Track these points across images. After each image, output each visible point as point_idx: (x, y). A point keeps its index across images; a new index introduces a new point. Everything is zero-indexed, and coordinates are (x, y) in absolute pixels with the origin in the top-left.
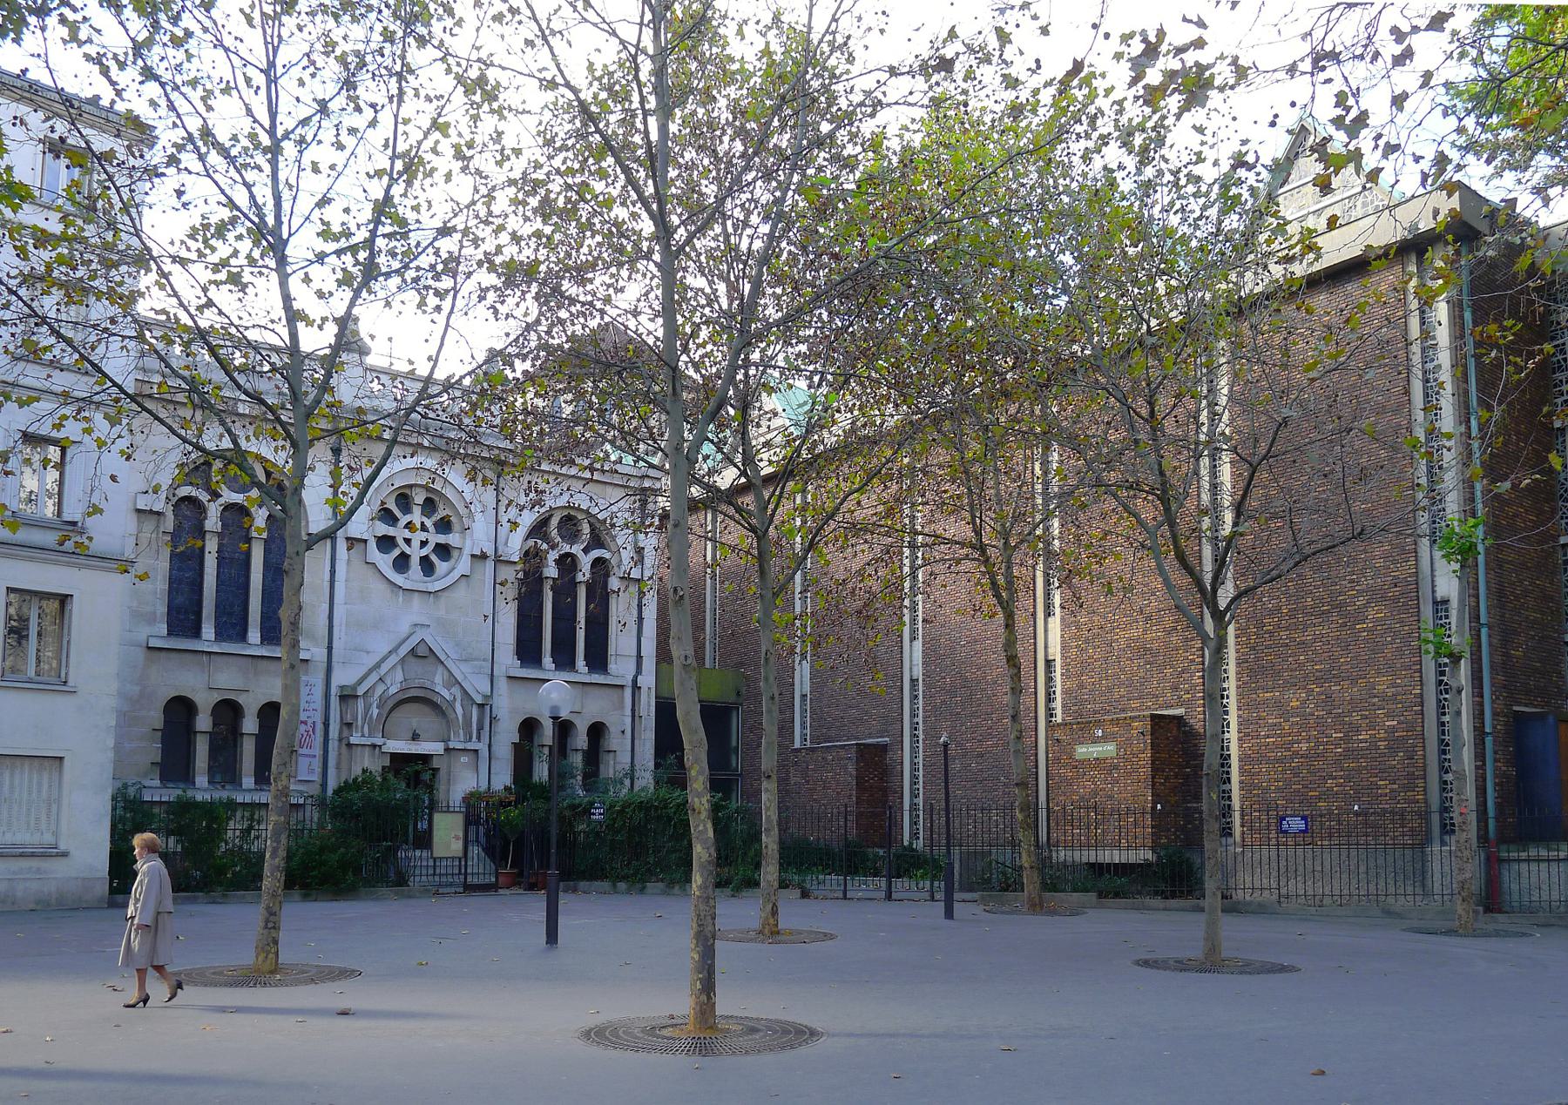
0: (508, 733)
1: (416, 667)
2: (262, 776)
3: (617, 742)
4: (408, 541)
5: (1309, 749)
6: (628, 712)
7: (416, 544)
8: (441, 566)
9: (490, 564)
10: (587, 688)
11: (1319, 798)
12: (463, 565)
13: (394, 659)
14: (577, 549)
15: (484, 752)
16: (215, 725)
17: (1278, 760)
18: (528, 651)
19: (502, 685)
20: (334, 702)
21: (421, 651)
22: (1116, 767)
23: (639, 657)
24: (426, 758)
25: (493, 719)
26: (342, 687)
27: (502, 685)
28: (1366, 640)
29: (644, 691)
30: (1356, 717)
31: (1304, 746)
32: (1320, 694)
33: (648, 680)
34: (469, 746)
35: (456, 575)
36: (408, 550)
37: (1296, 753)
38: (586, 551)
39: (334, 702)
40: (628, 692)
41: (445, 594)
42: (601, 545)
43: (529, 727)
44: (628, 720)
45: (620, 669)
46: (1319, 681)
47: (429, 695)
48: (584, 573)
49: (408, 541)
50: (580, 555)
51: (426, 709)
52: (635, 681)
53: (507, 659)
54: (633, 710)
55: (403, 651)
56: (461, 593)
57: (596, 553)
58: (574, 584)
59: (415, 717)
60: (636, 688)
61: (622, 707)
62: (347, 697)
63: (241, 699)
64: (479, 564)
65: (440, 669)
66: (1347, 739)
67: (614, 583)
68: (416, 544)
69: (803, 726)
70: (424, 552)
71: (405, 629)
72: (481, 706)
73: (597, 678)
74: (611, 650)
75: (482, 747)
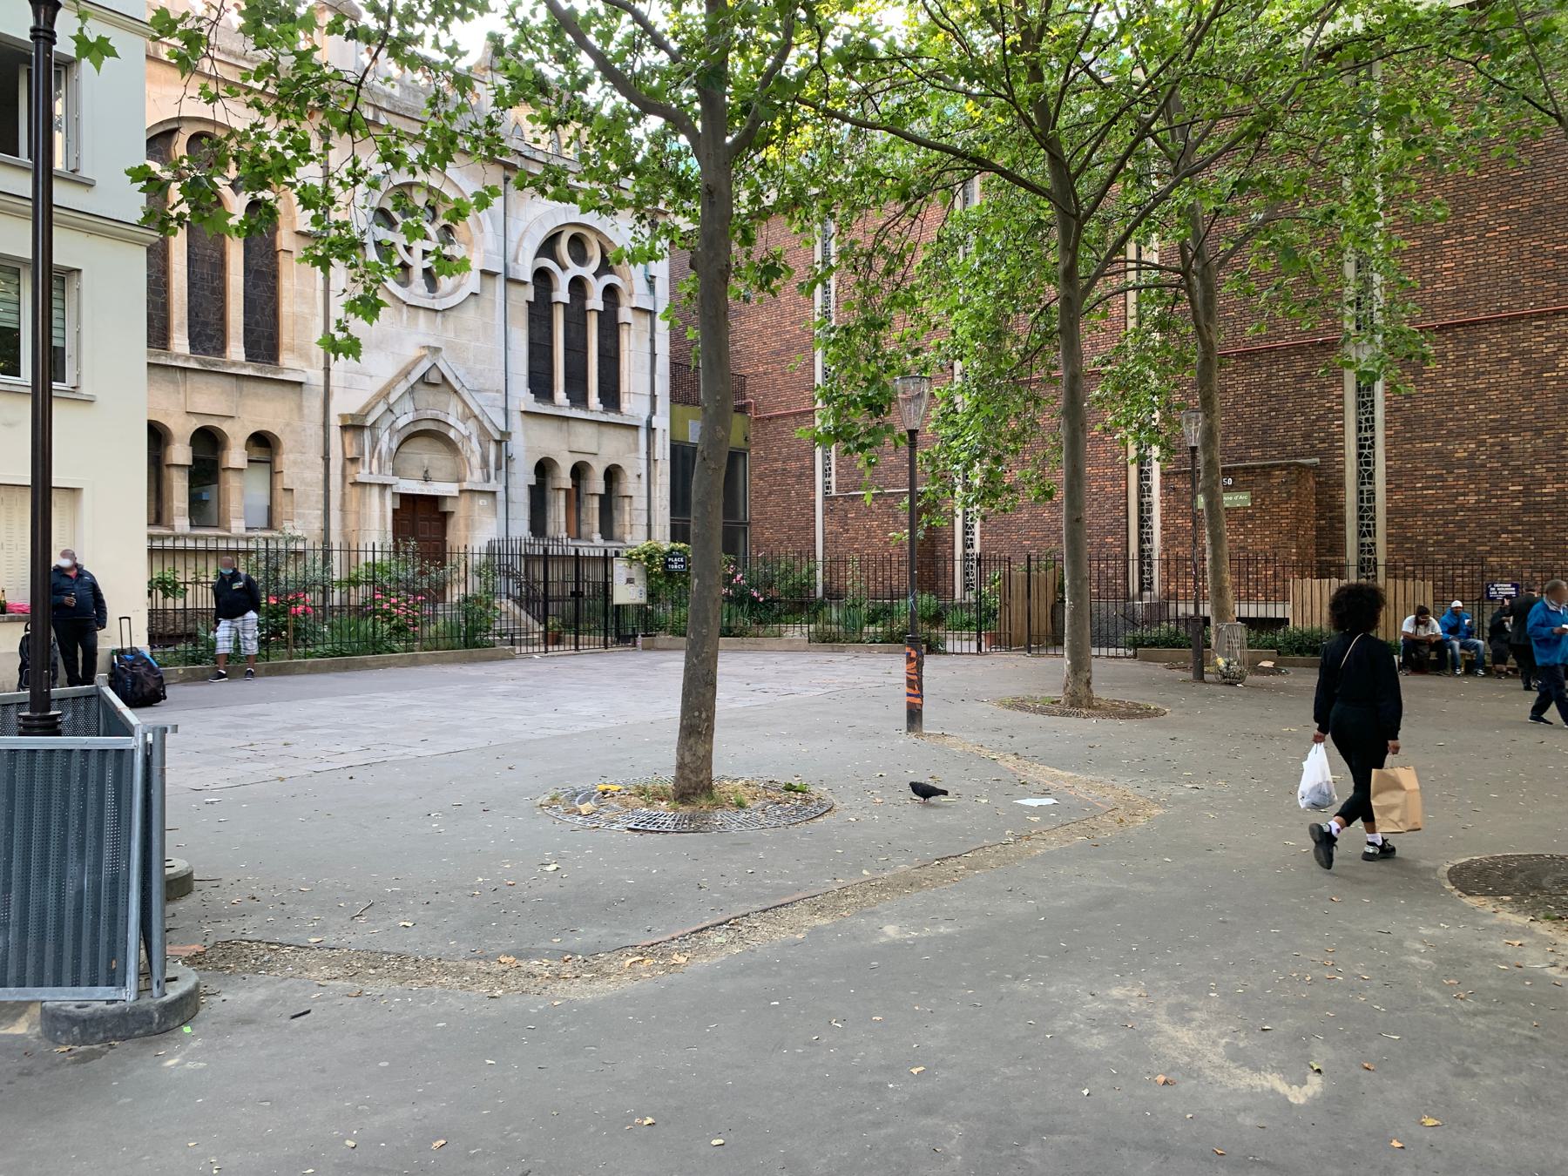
0: (523, 476)
1: (425, 394)
2: (607, 531)
3: (632, 485)
4: (408, 249)
5: (1478, 502)
6: (643, 455)
7: (417, 252)
8: (445, 283)
9: (500, 282)
10: (604, 429)
11: (1490, 553)
12: (472, 281)
13: (403, 387)
14: (587, 272)
15: (501, 496)
16: (195, 459)
17: (1436, 513)
18: (540, 384)
19: (517, 421)
20: (335, 432)
21: (434, 377)
22: (1251, 518)
23: (653, 397)
24: (435, 501)
25: (509, 458)
26: (343, 416)
27: (517, 421)
28: (1554, 390)
29: (659, 434)
30: (1540, 470)
31: (1472, 499)
32: (1493, 445)
33: (662, 422)
34: (487, 487)
35: (463, 293)
36: (409, 260)
37: (1462, 507)
38: (597, 275)
39: (335, 432)
40: (643, 434)
41: (454, 313)
42: (611, 271)
43: (544, 468)
44: (644, 464)
45: (633, 405)
46: (1492, 431)
47: (443, 429)
48: (595, 302)
49: (408, 249)
50: (591, 278)
51: (439, 445)
52: (649, 422)
53: (523, 398)
54: (648, 453)
55: (415, 375)
56: (470, 315)
57: (607, 279)
58: (584, 313)
59: (425, 454)
60: (651, 430)
61: (637, 450)
62: (353, 426)
63: (225, 427)
64: (489, 281)
65: (454, 400)
66: (1527, 492)
67: (625, 314)
68: (417, 252)
69: (827, 473)
70: (427, 264)
71: (412, 352)
72: (498, 443)
73: (612, 417)
74: (624, 387)
75: (500, 488)
